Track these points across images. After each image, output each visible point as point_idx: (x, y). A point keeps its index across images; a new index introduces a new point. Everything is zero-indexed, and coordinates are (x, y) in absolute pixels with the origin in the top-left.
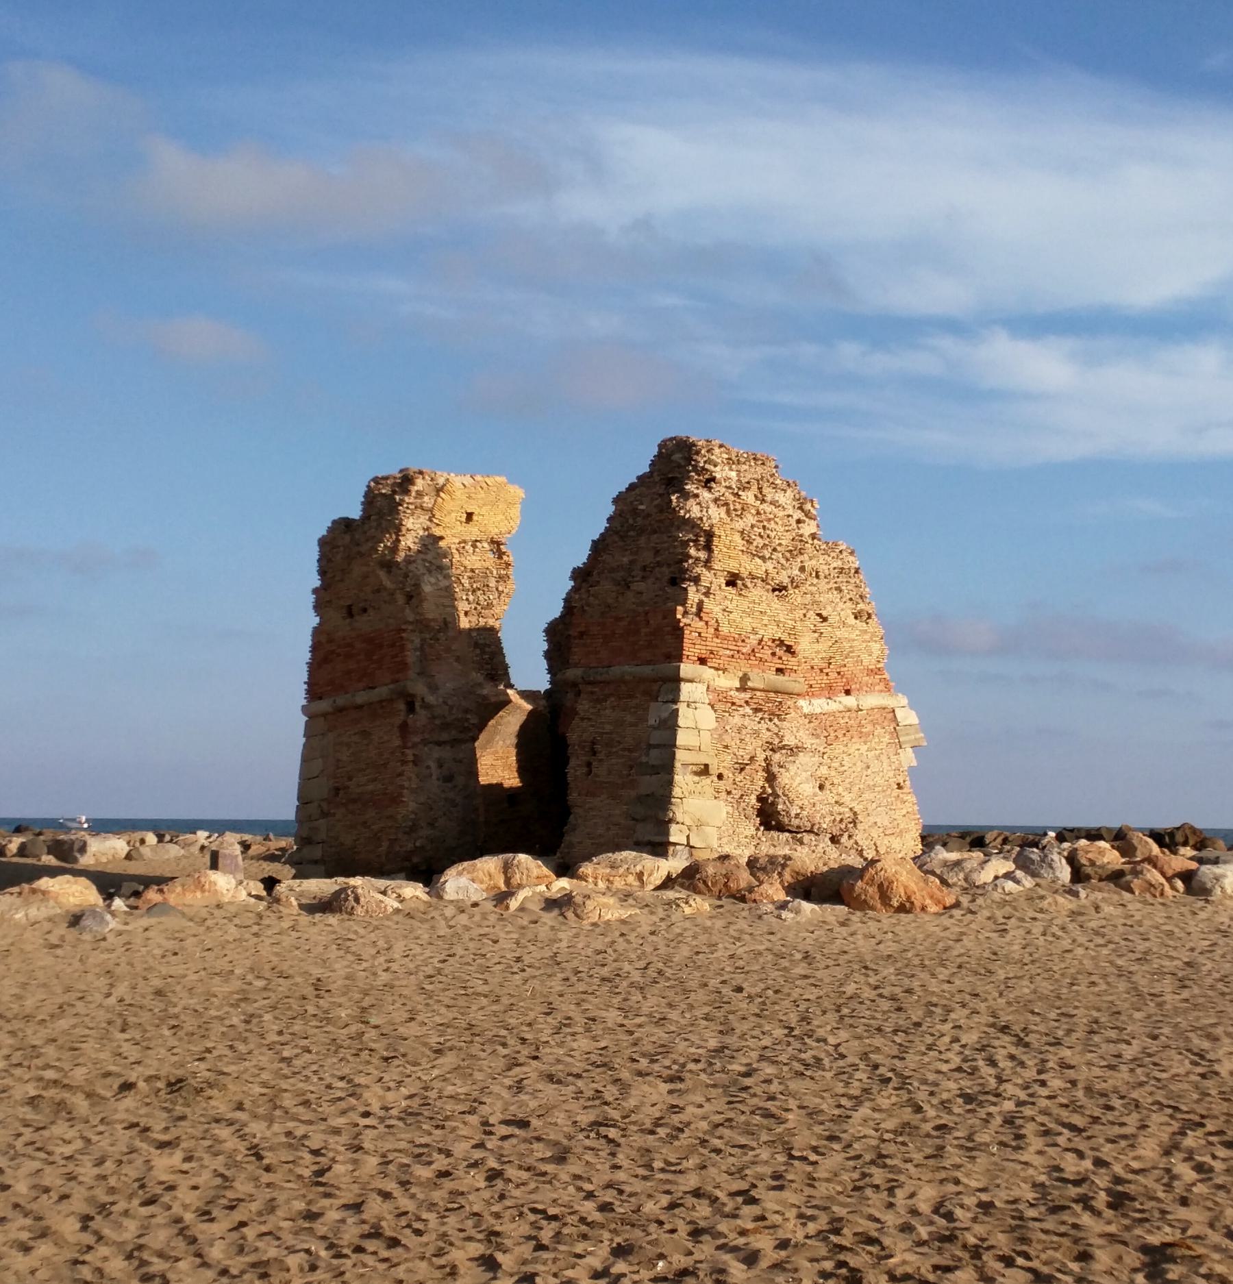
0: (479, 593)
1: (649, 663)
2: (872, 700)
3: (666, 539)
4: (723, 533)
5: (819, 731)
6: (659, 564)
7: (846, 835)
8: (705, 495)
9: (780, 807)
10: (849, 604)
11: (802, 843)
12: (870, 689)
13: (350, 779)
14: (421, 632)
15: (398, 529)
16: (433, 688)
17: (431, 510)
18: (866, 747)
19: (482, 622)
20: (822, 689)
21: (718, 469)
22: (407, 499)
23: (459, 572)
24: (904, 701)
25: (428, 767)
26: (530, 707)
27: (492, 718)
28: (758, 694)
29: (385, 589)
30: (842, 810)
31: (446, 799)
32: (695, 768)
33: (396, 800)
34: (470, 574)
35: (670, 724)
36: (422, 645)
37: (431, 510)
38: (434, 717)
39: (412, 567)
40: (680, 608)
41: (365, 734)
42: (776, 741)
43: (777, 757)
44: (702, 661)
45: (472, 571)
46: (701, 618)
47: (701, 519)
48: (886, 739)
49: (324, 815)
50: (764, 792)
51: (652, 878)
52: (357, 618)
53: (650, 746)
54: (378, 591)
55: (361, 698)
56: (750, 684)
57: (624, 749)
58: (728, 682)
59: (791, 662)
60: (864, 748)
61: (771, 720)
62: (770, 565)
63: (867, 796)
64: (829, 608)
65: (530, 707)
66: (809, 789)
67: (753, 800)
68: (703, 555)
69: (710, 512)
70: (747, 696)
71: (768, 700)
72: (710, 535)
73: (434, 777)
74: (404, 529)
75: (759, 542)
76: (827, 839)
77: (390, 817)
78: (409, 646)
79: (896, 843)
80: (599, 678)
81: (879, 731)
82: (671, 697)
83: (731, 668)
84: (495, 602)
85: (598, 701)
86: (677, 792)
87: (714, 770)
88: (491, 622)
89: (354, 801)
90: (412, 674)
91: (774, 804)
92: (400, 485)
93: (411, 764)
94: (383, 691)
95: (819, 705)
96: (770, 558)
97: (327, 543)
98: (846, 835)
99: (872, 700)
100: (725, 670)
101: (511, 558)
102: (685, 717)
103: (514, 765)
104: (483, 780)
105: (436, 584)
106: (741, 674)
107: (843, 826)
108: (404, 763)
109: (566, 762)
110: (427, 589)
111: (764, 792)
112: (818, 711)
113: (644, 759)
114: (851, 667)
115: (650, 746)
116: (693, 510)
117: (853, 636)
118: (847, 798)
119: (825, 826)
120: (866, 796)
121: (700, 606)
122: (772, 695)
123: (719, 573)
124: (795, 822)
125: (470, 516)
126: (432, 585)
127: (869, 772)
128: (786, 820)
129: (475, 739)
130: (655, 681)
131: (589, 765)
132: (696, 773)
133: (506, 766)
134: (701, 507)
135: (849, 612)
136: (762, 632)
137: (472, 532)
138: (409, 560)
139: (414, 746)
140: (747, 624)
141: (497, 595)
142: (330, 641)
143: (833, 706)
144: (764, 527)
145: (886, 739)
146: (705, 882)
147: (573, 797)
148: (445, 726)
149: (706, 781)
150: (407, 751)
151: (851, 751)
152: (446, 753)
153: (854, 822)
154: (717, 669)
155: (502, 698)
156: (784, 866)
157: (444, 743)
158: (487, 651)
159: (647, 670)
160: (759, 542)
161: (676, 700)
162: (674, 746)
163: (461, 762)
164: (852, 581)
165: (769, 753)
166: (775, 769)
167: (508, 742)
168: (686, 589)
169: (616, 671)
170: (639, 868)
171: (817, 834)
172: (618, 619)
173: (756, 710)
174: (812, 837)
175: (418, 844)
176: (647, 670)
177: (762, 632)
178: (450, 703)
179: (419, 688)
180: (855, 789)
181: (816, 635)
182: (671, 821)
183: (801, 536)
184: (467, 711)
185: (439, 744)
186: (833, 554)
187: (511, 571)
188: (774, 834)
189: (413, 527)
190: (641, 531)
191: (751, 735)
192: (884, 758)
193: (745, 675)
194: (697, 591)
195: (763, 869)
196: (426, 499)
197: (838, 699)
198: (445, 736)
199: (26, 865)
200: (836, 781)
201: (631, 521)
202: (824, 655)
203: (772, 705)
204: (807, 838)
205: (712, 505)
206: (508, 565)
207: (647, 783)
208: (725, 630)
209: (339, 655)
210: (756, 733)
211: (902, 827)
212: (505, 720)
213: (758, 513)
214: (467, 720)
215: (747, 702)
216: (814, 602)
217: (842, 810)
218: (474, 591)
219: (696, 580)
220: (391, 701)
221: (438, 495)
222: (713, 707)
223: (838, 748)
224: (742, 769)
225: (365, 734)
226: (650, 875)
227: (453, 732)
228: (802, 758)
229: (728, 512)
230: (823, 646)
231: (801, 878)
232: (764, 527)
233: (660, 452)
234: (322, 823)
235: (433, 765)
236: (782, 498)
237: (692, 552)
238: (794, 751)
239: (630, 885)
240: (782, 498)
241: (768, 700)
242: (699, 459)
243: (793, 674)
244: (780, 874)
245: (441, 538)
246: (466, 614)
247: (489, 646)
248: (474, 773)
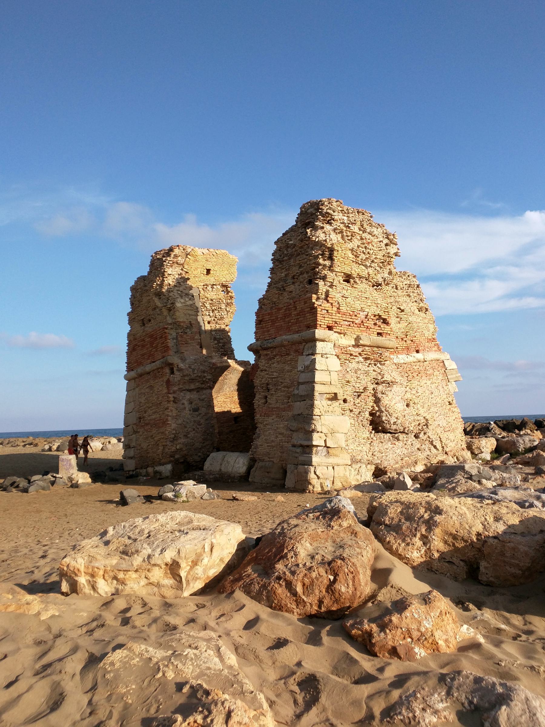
0: (216, 312)
1: (297, 332)
2: (432, 355)
3: (305, 257)
4: (340, 249)
5: (403, 374)
6: (302, 273)
7: (422, 432)
8: (328, 227)
9: (384, 418)
10: (415, 304)
11: (398, 440)
12: (430, 349)
14: (176, 329)
16: (183, 360)
17: (183, 265)
18: (430, 382)
19: (218, 327)
20: (403, 350)
21: (336, 214)
22: (168, 258)
23: (204, 300)
24: (448, 357)
25: (183, 404)
26: (242, 369)
27: (221, 376)
28: (367, 348)
29: (158, 307)
30: (419, 418)
31: (195, 421)
32: (328, 396)
33: (165, 423)
34: (211, 302)
35: (311, 369)
36: (177, 336)
37: (183, 265)
38: (184, 376)
39: (171, 294)
40: (314, 296)
41: (151, 387)
42: (380, 377)
43: (380, 388)
44: (330, 328)
45: (212, 300)
46: (328, 301)
47: (326, 241)
48: (440, 377)
49: (135, 432)
50: (373, 410)
51: (199, 570)
52: (146, 325)
53: (299, 384)
54: (155, 309)
55: (148, 368)
56: (361, 342)
57: (285, 387)
58: (347, 341)
59: (386, 329)
60: (429, 382)
61: (375, 365)
62: (371, 271)
63: (433, 409)
64: (404, 305)
65: (242, 369)
66: (401, 406)
67: (367, 414)
68: (328, 263)
69: (331, 236)
70: (359, 350)
71: (373, 353)
72: (331, 250)
73: (187, 409)
74: (166, 273)
75: (363, 256)
76: (413, 436)
77: (162, 433)
78: (170, 337)
79: (451, 436)
80: (269, 345)
81: (436, 373)
82: (310, 352)
83: (348, 333)
84: (225, 316)
85: (270, 359)
86: (316, 411)
87: (340, 397)
88: (223, 327)
89: (147, 424)
90: (171, 352)
91: (379, 416)
92: (168, 253)
93: (172, 402)
94: (158, 364)
95: (402, 358)
96: (370, 266)
97: (134, 289)
98: (422, 432)
99: (432, 355)
100: (345, 334)
101: (233, 294)
102: (320, 363)
103: (237, 401)
104: (217, 410)
105: (184, 303)
106: (355, 336)
107: (420, 428)
108: (169, 402)
109: (254, 396)
110: (178, 305)
111: (373, 410)
112: (402, 361)
113: (296, 392)
114: (419, 338)
115: (299, 384)
116: (320, 236)
117: (418, 320)
118: (422, 412)
119: (412, 429)
120: (432, 409)
121: (327, 294)
122: (375, 349)
123: (338, 274)
124: (394, 427)
125: (208, 271)
126: (182, 303)
127: (433, 396)
128: (388, 426)
129: (212, 388)
130: (300, 343)
131: (266, 397)
132: (330, 399)
133: (232, 402)
134: (326, 234)
135: (416, 307)
136: (367, 310)
137: (210, 280)
138: (169, 291)
139: (174, 392)
140: (358, 305)
141: (226, 313)
142: (135, 339)
143: (410, 359)
144: (366, 248)
145: (440, 377)
146: (289, 586)
147: (257, 417)
148: (192, 381)
149: (336, 404)
150: (170, 395)
151: (422, 384)
152: (194, 396)
153: (426, 425)
154: (340, 333)
155: (224, 364)
156: (430, 524)
157: (193, 390)
158: (222, 342)
159: (296, 336)
160: (363, 256)
161: (313, 354)
162: (314, 382)
163: (203, 400)
164: (416, 291)
165: (375, 386)
166: (380, 395)
167: (232, 389)
168: (318, 284)
169: (279, 339)
170: (169, 555)
171: (407, 434)
172: (279, 309)
173: (366, 359)
174: (404, 435)
175: (178, 447)
176: (296, 336)
177: (367, 310)
178: (193, 367)
179: (175, 360)
180: (426, 406)
181: (398, 319)
182: (313, 431)
183: (389, 253)
184: (204, 372)
185: (190, 391)
186: (404, 277)
187: (233, 301)
188: (381, 435)
189: (172, 275)
190: (291, 256)
191: (363, 374)
192: (440, 387)
193: (358, 336)
194: (325, 285)
195: (396, 528)
196: (179, 258)
197: (412, 355)
198: (192, 387)
199: (48, 454)
200: (416, 402)
201: (285, 252)
202: (403, 330)
203: (375, 355)
204: (401, 436)
205: (332, 233)
206: (231, 297)
207: (299, 407)
208: (343, 309)
210: (367, 373)
211: (453, 426)
212: (229, 377)
213: (362, 239)
214: (204, 377)
215: (360, 354)
216: (396, 302)
217: (419, 418)
218: (213, 311)
219: (324, 278)
220: (162, 368)
221: (187, 257)
222: (338, 357)
223: (415, 383)
224: (359, 396)
225: (151, 387)
226: (195, 563)
227: (197, 384)
228: (395, 388)
229: (342, 237)
230: (403, 325)
231: (460, 545)
232: (366, 248)
233: (301, 211)
235: (186, 403)
236: (376, 231)
237: (321, 261)
238: (389, 384)
239: (158, 585)
240: (376, 231)
241: (373, 353)
242: (323, 207)
243: (388, 336)
244: (425, 540)
245: (188, 279)
246: (209, 323)
247: (222, 339)
248: (212, 406)
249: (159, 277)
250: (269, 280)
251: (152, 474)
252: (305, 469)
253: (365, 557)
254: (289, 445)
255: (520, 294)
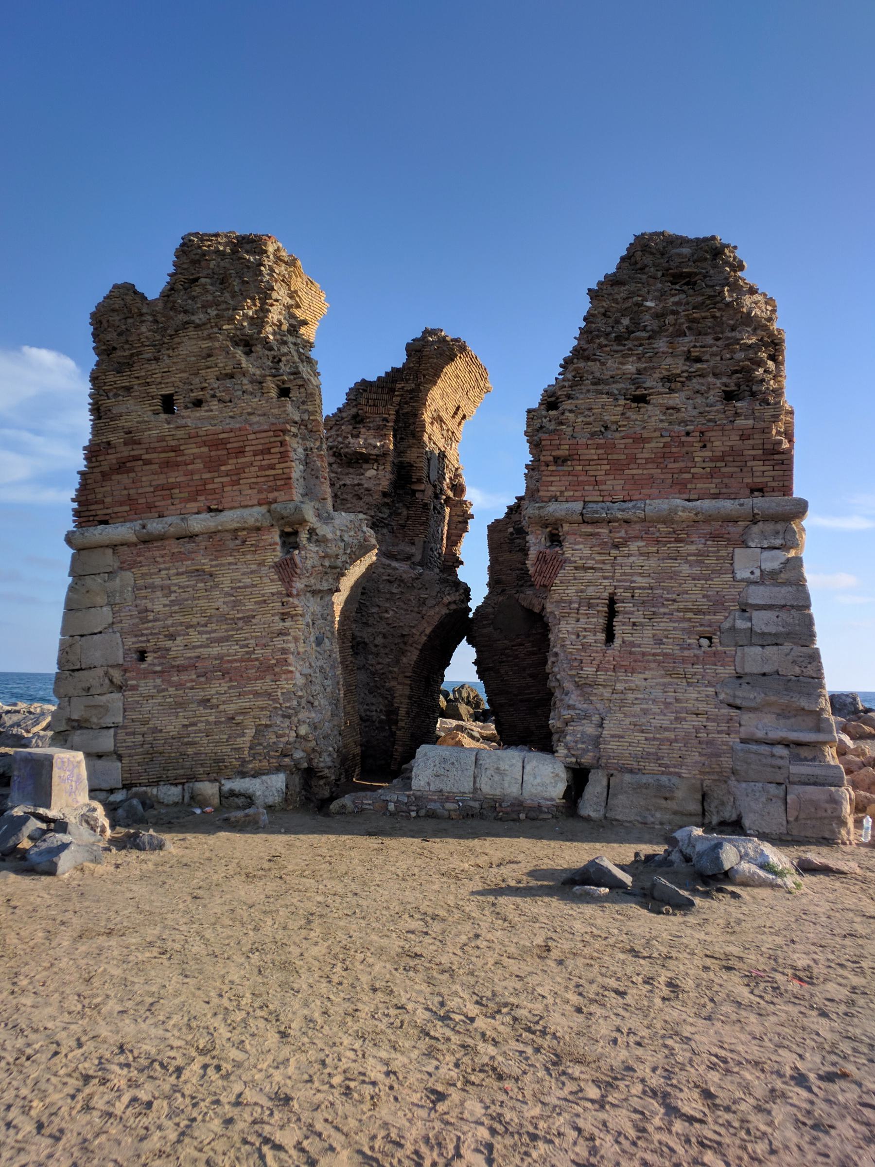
13: (172, 637)
14: (303, 439)
15: (265, 294)
33: (272, 669)
55: (199, 523)
89: (181, 669)
209: (148, 462)
234: (115, 699)
249: (253, 299)
250: (576, 342)
251: (216, 801)
252: (831, 794)
253: (116, 1068)
254: (734, 739)
255: (374, 789)
